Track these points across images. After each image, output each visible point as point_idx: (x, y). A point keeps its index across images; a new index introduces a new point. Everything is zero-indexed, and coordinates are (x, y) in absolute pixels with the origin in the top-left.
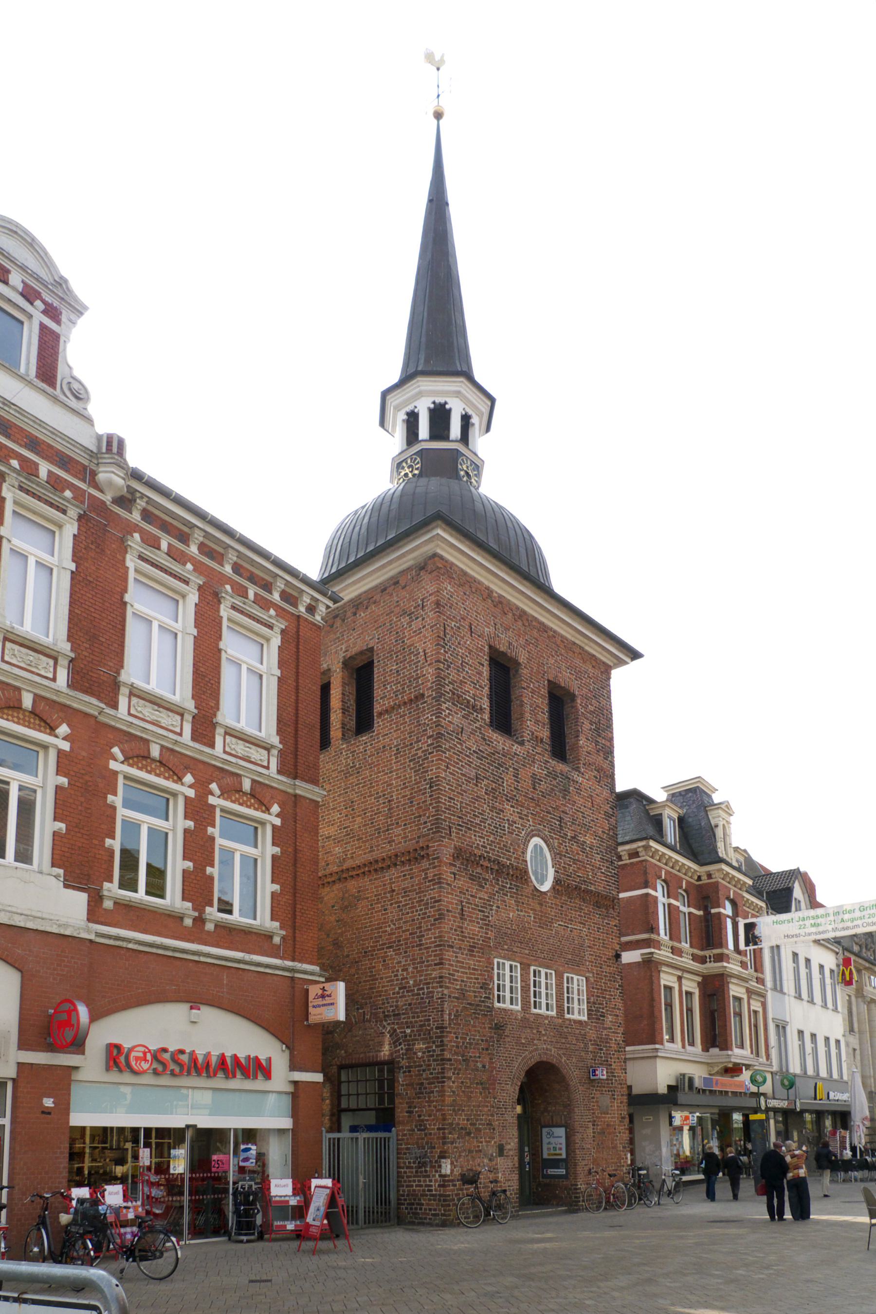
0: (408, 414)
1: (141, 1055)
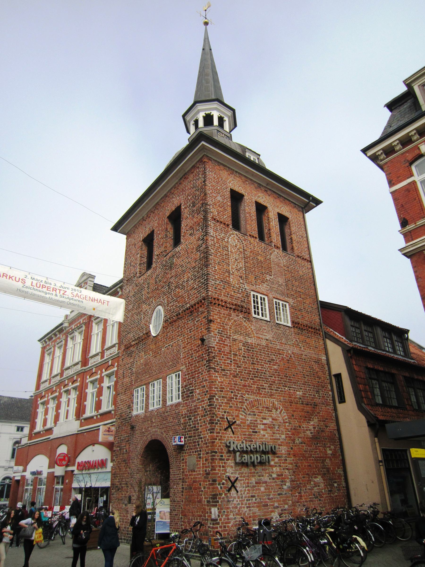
0: (195, 121)
1: (62, 458)
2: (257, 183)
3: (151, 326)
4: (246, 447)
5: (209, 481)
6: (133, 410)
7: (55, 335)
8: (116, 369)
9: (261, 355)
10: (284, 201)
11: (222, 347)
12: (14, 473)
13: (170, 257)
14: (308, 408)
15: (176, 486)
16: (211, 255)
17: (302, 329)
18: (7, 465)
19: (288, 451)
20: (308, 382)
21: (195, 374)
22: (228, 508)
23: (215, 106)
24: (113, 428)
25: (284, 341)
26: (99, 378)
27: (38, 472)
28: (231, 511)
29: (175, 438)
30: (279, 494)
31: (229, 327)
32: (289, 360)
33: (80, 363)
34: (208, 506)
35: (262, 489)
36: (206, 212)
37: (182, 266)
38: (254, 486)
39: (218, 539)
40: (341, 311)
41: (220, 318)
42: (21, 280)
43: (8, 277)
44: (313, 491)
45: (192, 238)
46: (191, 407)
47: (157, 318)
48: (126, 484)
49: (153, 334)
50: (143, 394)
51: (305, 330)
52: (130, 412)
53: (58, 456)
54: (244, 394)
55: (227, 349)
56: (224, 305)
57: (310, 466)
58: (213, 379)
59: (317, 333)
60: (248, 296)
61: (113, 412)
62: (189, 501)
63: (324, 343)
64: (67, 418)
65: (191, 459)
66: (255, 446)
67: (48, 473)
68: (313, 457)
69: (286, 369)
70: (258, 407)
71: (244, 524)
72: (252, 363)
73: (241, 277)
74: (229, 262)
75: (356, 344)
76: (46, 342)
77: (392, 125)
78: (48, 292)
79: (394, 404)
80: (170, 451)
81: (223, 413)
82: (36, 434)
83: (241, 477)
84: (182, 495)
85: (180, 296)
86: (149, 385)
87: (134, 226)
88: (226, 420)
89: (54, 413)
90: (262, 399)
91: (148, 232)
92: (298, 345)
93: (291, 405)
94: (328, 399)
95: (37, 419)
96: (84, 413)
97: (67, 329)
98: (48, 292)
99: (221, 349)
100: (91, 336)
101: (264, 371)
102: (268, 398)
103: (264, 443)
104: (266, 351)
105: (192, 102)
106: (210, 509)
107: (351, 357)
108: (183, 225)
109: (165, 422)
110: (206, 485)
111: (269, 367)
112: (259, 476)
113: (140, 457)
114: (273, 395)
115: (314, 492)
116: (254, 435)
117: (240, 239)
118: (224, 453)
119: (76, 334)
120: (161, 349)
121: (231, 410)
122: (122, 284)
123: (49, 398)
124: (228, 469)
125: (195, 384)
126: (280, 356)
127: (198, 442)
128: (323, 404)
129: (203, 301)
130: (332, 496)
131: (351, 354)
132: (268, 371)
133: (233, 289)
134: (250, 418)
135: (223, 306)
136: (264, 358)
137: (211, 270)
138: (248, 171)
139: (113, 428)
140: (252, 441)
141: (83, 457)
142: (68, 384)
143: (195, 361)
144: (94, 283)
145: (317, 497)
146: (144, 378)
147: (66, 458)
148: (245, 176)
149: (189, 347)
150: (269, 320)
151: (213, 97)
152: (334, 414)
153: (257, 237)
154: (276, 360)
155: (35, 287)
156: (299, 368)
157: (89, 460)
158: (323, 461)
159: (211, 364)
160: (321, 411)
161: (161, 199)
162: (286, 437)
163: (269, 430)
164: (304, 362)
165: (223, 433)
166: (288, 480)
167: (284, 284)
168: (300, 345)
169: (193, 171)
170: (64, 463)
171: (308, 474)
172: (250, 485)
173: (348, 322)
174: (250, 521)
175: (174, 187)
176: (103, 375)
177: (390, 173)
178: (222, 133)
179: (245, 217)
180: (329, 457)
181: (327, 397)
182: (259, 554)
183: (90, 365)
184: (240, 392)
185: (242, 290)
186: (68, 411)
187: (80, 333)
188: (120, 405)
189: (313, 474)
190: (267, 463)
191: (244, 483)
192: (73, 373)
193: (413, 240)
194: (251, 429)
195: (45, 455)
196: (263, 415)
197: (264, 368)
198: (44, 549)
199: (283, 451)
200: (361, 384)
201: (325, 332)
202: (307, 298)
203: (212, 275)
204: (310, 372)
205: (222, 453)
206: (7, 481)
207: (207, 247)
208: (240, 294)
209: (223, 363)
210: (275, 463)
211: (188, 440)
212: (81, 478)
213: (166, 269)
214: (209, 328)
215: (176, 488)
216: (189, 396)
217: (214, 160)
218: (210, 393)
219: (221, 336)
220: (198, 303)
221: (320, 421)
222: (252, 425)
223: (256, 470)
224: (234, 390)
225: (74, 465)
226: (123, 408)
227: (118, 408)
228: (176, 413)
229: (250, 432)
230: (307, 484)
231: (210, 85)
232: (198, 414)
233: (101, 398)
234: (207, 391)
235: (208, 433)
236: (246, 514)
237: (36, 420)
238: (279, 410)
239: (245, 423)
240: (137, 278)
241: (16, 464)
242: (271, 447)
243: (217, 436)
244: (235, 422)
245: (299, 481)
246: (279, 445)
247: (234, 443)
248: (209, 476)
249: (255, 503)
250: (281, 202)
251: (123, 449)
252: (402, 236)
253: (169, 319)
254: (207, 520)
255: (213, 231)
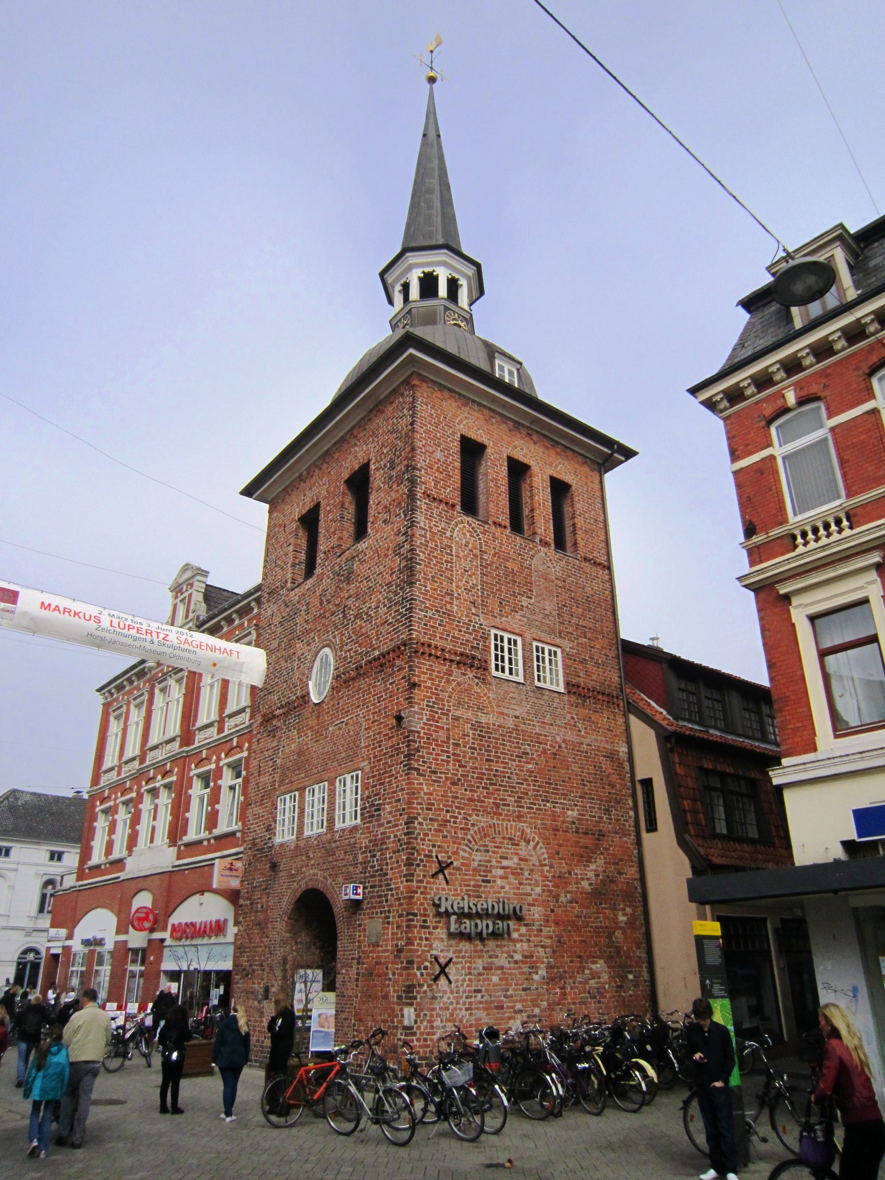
1: (143, 915)
2: (512, 420)
3: (311, 684)
4: (469, 908)
5: (402, 963)
6: (275, 834)
7: (131, 682)
8: (245, 754)
9: (504, 745)
10: (563, 454)
11: (434, 731)
12: (49, 941)
13: (347, 560)
14: (584, 841)
15: (347, 971)
16: (420, 564)
17: (584, 696)
18: (30, 925)
19: (544, 915)
20: (591, 794)
21: (385, 778)
22: (433, 1009)
23: (443, 258)
24: (239, 865)
25: (548, 719)
26: (214, 770)
27: (95, 939)
28: (438, 1015)
29: (346, 887)
30: (524, 990)
31: (447, 694)
32: (555, 754)
33: (178, 739)
34: (398, 1004)
35: (495, 979)
36: (413, 482)
37: (368, 579)
38: (480, 974)
39: (405, 1054)
40: (661, 662)
41: (433, 680)
42: (93, 618)
43: (72, 613)
44: (587, 987)
45: (388, 528)
46: (377, 835)
47: (321, 670)
48: (261, 965)
49: (315, 699)
50: (294, 806)
51: (589, 697)
52: (270, 839)
53: (137, 911)
54: (470, 815)
55: (442, 735)
56: (441, 656)
57: (584, 941)
58: (415, 788)
59: (613, 704)
60: (485, 638)
61: (239, 835)
62: (368, 996)
63: (625, 722)
64: (152, 841)
65: (372, 925)
66: (485, 906)
67: (116, 942)
68: (592, 927)
69: (549, 771)
70: (494, 838)
71: (461, 1036)
72: (487, 760)
73: (474, 603)
74: (452, 575)
75: (685, 724)
76: (112, 695)
77: (746, 345)
78: (139, 635)
79: (751, 835)
80: (338, 909)
81: (431, 848)
82: (90, 868)
83: (458, 957)
84: (357, 986)
85: (363, 635)
86: (304, 791)
87: (284, 490)
88: (435, 859)
89: (128, 831)
90: (502, 825)
91: (309, 506)
92: (575, 726)
93: (555, 835)
94: (627, 824)
95: (93, 840)
96: (185, 833)
97: (153, 672)
98: (139, 635)
99: (431, 735)
100: (199, 689)
101: (507, 773)
102: (514, 821)
103: (501, 900)
104: (515, 738)
105: (398, 250)
106: (402, 1010)
107: (672, 750)
108: (371, 502)
109: (330, 859)
110: (397, 969)
111: (517, 766)
112: (490, 957)
113: (286, 919)
114: (522, 816)
115: (590, 988)
116: (485, 886)
117: (476, 532)
118: (428, 916)
119: (171, 682)
120: (328, 729)
121: (445, 842)
122: (259, 593)
123: (118, 801)
124: (436, 944)
125: (384, 795)
126: (539, 747)
127: (386, 895)
128: (616, 833)
129: (403, 648)
130: (622, 997)
131: (672, 744)
132: (516, 774)
133: (457, 626)
134: (478, 857)
135: (437, 657)
136: (509, 750)
137: (417, 591)
138: (494, 400)
139: (239, 865)
140: (481, 897)
141: (181, 916)
142: (154, 778)
143: (385, 754)
144: (207, 585)
145: (595, 997)
146: (296, 778)
147: (151, 917)
148: (490, 409)
149: (375, 727)
150: (522, 681)
151: (441, 241)
152: (635, 851)
153: (508, 524)
154: (533, 754)
155: (117, 629)
156: (575, 768)
157: (194, 921)
158: (610, 936)
159: (412, 762)
160: (611, 846)
161: (335, 444)
162: (543, 891)
163: (511, 878)
164: (585, 756)
165: (428, 883)
166: (542, 966)
167: (555, 613)
168: (580, 726)
169: (392, 399)
170: (147, 925)
171: (580, 957)
172: (472, 971)
173: (674, 683)
174: (471, 1032)
175: (358, 425)
176: (221, 764)
177: (734, 437)
178: (454, 312)
179: (487, 487)
180: (621, 928)
181: (624, 820)
182: (467, 1078)
183: (197, 745)
184: (462, 812)
185: (474, 626)
186: (154, 828)
187: (179, 681)
188: (252, 824)
189: (588, 958)
190: (506, 936)
191: (463, 968)
192: (164, 757)
193: (761, 562)
194: (480, 875)
195: (111, 910)
196: (503, 853)
197: (509, 768)
198: (117, 1074)
199: (536, 916)
200: (687, 799)
201: (628, 703)
202: (597, 639)
203: (420, 601)
204: (595, 774)
205: (425, 915)
206: (31, 956)
207: (412, 550)
208: (471, 634)
209: (434, 759)
210: (520, 935)
211: (369, 892)
212: (180, 951)
213: (340, 581)
214: (411, 698)
215: (347, 974)
216: (373, 816)
217: (431, 380)
218: (408, 813)
219: (431, 711)
220: (394, 651)
221: (609, 863)
222: (482, 868)
223: (484, 946)
224: (451, 806)
225: (164, 929)
226: (257, 828)
227: (249, 829)
228: (350, 845)
229: (478, 880)
230: (578, 973)
231: (434, 212)
232: (387, 849)
233: (217, 806)
234: (404, 809)
235: (402, 882)
236: (465, 1021)
237: (92, 843)
238: (532, 844)
239: (469, 865)
240: (288, 590)
241: (53, 926)
242: (515, 909)
243: (419, 887)
244: (452, 863)
245: (563, 967)
246: (529, 905)
247: (447, 899)
248: (403, 955)
249: (481, 1003)
250: (557, 454)
251: (257, 903)
252: (744, 553)
253: (344, 673)
254: (397, 1028)
255: (426, 518)
